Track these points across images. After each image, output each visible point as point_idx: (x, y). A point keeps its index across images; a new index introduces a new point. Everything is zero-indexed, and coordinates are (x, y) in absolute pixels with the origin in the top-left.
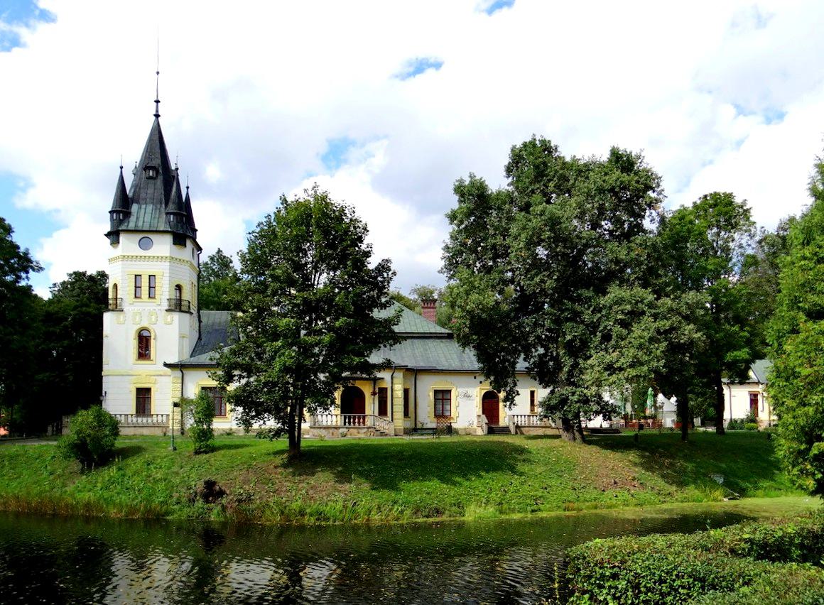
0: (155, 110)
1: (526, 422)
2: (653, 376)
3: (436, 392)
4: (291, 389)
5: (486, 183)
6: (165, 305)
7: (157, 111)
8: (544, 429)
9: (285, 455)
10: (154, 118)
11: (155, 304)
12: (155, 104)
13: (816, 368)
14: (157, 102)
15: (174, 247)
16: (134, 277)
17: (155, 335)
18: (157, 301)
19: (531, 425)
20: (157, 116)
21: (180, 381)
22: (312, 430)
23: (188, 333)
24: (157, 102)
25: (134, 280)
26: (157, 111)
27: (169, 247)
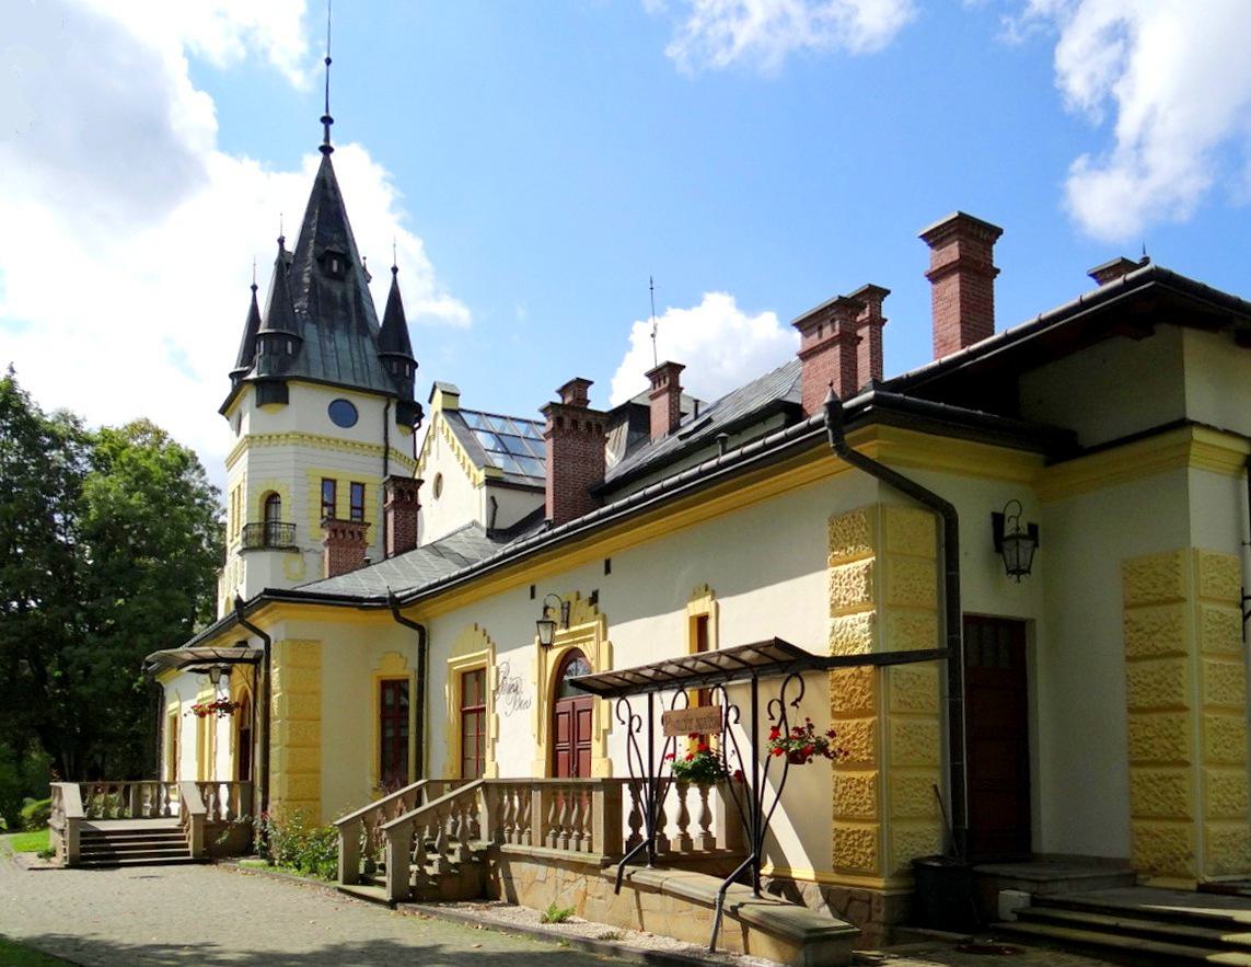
0: (323, 136)
7: (327, 139)
14: (327, 120)
15: (258, 411)
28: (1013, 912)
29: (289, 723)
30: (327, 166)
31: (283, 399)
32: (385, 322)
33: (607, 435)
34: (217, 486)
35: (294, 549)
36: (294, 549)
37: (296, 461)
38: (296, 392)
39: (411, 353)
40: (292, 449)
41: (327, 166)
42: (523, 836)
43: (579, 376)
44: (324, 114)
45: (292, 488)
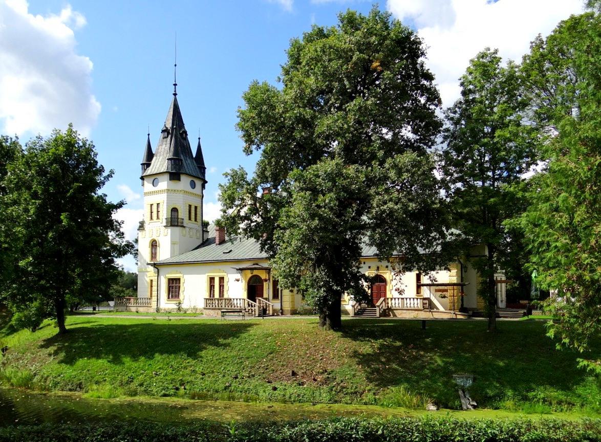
0: (174, 90)
1: (400, 305)
2: (347, 237)
3: (169, 280)
4: (43, 282)
5: (566, 18)
6: (164, 224)
7: (175, 91)
8: (417, 312)
9: (432, 317)
10: (173, 96)
11: (159, 223)
12: (174, 86)
13: (321, 177)
14: (175, 85)
15: (170, 182)
16: (150, 206)
17: (159, 244)
18: (161, 221)
19: (405, 308)
20: (175, 95)
21: (157, 275)
22: (205, 310)
23: (178, 241)
24: (175, 85)
25: (150, 208)
26: (175, 91)
27: (166, 182)
28: (362, 267)
29: (263, 252)
30: (175, 100)
31: (179, 179)
32: (196, 155)
33: (534, 386)
34: (104, 186)
35: (184, 227)
36: (184, 227)
37: (184, 199)
38: (183, 177)
39: (204, 165)
40: (182, 195)
41: (175, 100)
42: (316, 324)
43: (562, 20)
44: (174, 83)
45: (182, 207)
